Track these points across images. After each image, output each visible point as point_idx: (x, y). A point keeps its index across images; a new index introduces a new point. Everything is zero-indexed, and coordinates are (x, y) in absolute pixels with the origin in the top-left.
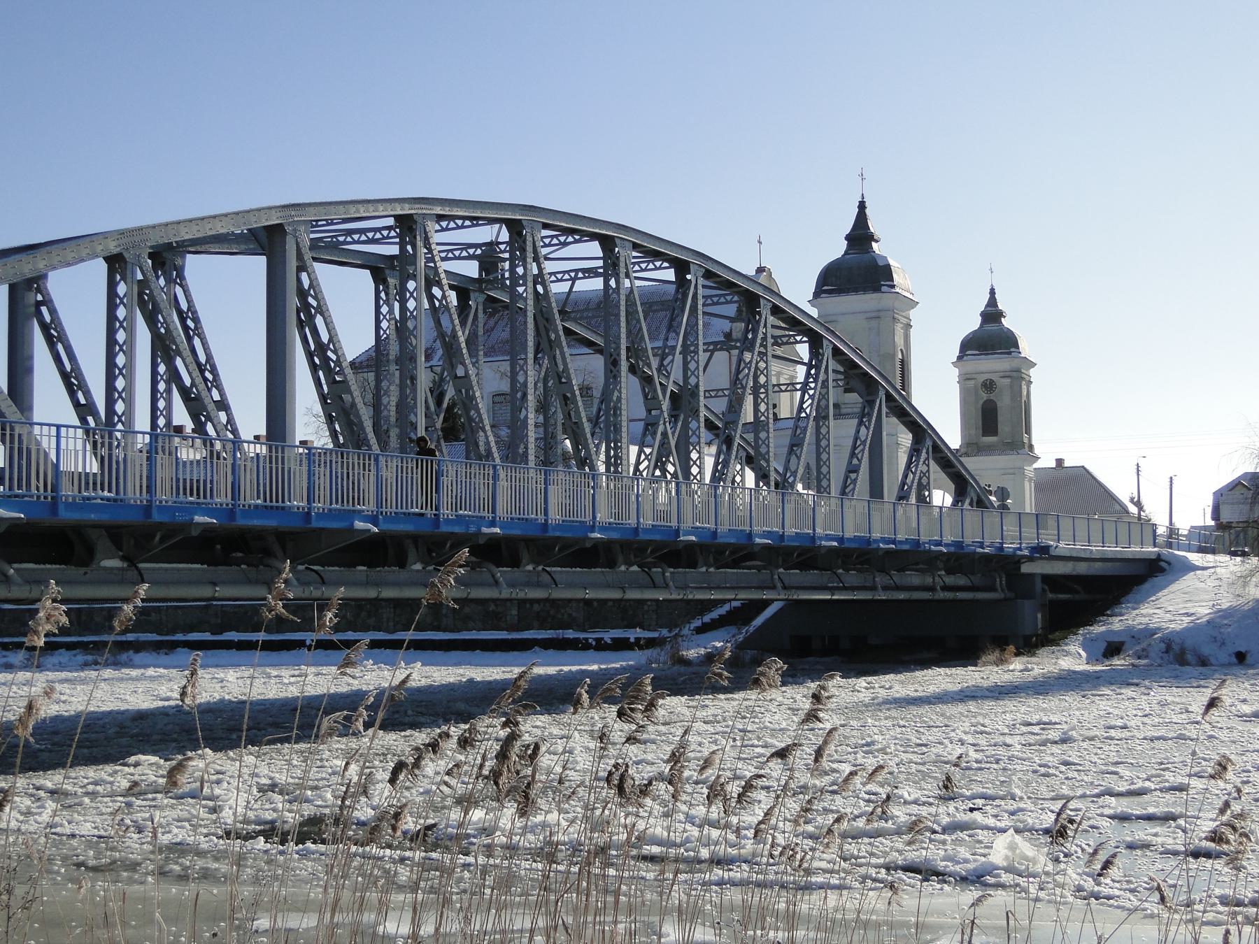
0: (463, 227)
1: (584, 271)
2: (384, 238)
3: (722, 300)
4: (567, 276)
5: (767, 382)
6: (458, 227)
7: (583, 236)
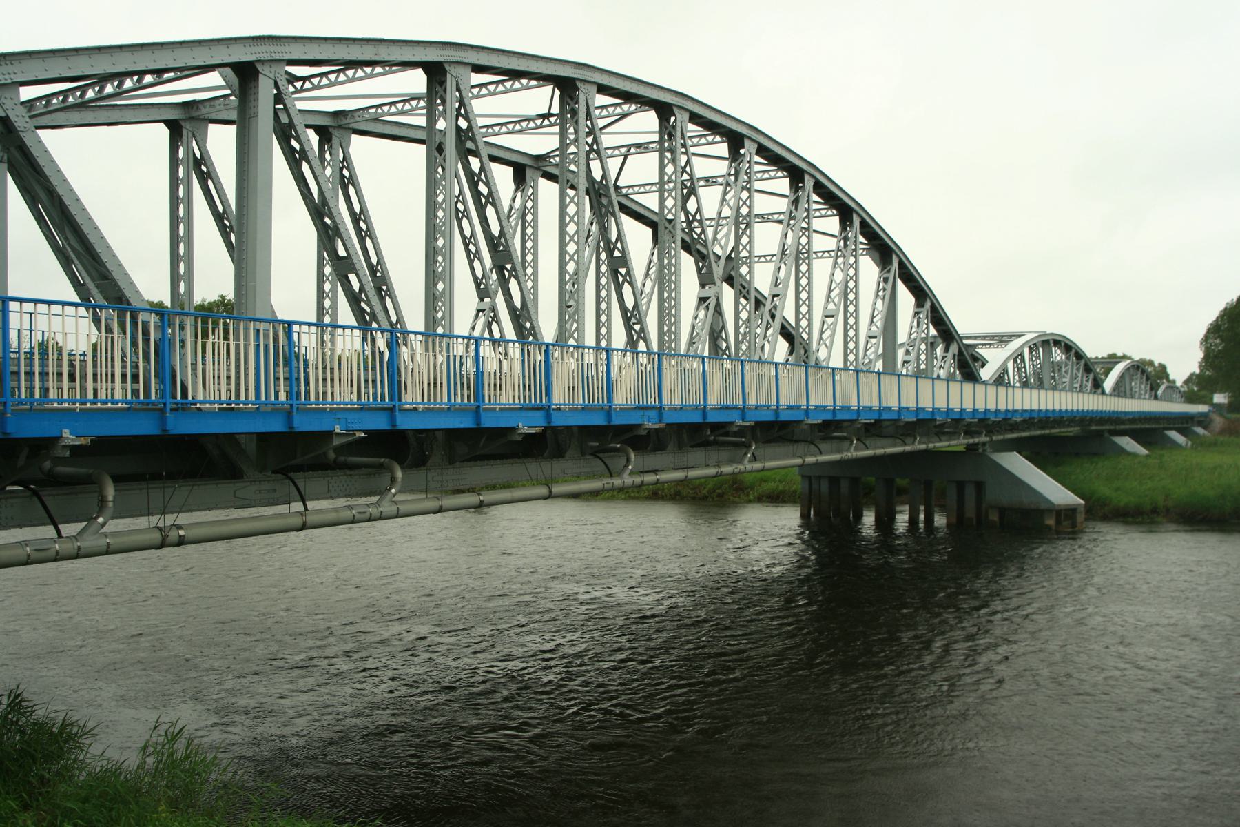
0: (372, 76)
1: (638, 146)
2: (519, 122)
3: (851, 345)
4: (617, 152)
5: (750, 212)
6: (367, 77)
7: (391, 66)
